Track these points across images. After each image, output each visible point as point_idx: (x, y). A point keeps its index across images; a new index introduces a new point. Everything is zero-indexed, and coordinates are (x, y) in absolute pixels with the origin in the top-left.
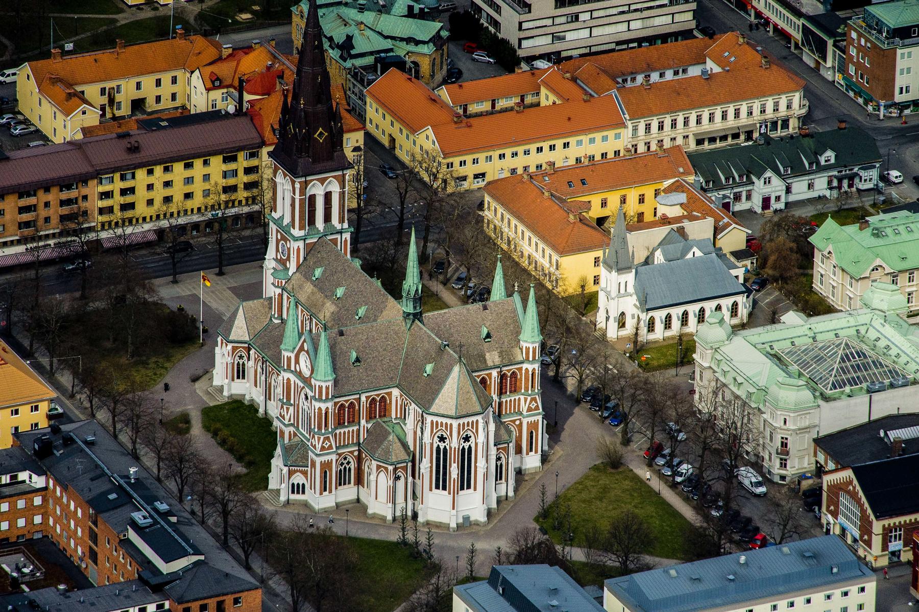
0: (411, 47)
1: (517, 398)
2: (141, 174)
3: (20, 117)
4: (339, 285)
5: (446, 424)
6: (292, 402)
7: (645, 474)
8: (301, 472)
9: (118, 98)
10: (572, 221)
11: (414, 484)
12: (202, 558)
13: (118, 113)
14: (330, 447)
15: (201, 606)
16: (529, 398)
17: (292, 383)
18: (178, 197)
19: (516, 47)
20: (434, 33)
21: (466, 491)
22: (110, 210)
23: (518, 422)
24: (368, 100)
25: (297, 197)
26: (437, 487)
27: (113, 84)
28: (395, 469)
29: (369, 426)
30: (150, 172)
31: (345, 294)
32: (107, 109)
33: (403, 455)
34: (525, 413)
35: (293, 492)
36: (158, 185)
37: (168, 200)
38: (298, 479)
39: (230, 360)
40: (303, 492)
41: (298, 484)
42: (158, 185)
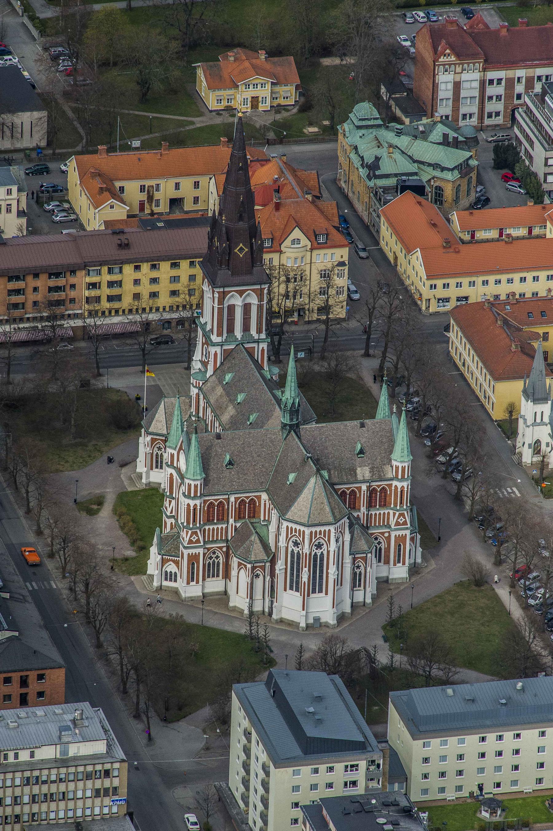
0: (437, 173)
1: (386, 512)
2: (128, 269)
3: (66, 206)
4: (241, 392)
5: (300, 530)
6: (174, 496)
7: (503, 593)
8: (174, 561)
9: (157, 195)
10: (513, 350)
11: (272, 582)
12: (17, 634)
13: (156, 210)
14: (198, 541)
15: (38, 675)
16: (397, 513)
17: (174, 478)
18: (145, 295)
19: (542, 180)
20: (461, 161)
21: (317, 595)
22: (98, 299)
23: (386, 535)
24: (382, 219)
25: (216, 305)
26: (291, 588)
27: (153, 182)
28: (253, 568)
29: (238, 525)
30: (137, 268)
31: (244, 400)
32: (147, 205)
33: (262, 555)
34: (393, 527)
35: (166, 579)
36: (145, 281)
37: (154, 295)
38: (171, 568)
39: (148, 450)
40: (175, 581)
41: (171, 572)
42: (145, 281)
